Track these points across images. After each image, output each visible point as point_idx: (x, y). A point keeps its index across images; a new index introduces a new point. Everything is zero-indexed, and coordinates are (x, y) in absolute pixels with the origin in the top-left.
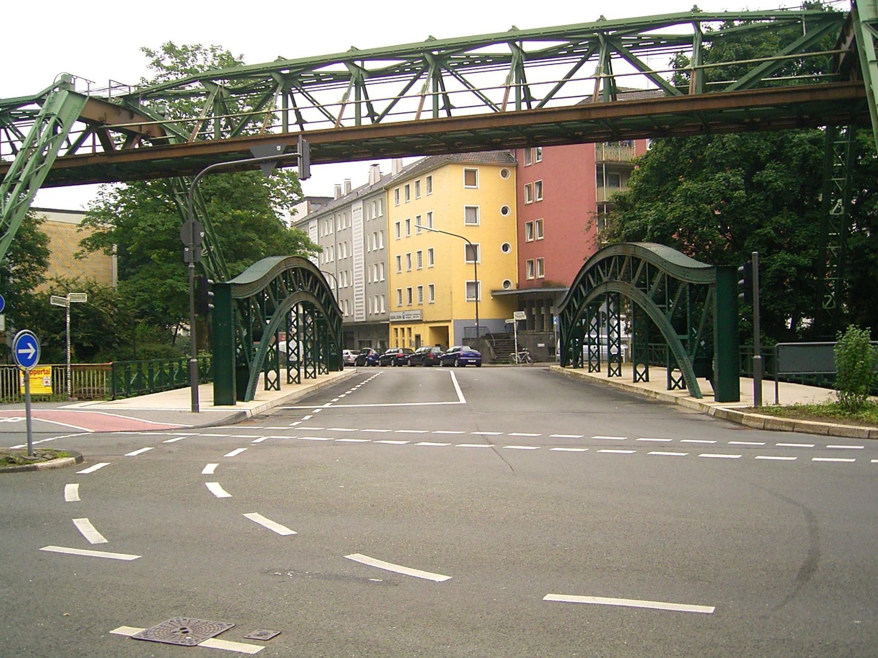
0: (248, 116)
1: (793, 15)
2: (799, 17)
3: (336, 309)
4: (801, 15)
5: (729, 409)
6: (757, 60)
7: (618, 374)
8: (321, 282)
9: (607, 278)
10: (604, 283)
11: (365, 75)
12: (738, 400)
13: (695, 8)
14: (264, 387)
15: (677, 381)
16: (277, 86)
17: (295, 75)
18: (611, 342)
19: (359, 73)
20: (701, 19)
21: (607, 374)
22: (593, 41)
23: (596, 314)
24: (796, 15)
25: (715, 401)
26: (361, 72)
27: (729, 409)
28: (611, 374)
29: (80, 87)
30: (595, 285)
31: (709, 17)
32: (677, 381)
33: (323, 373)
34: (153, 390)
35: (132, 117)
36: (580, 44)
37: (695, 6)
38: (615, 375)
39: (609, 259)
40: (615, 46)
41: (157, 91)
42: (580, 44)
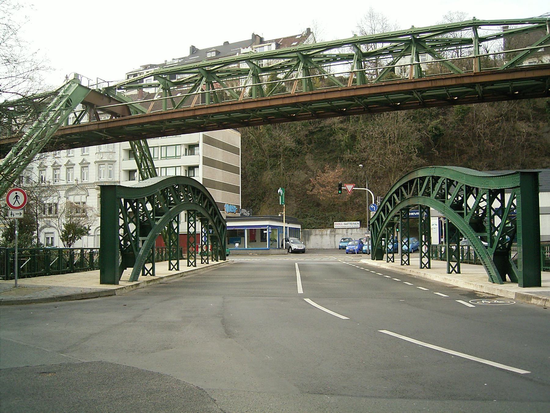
0: (185, 96)
1: (540, 21)
2: (544, 22)
3: (220, 217)
4: (545, 21)
5: (527, 292)
6: (100, 133)
7: (407, 264)
8: (208, 198)
9: (409, 195)
10: (407, 199)
11: (258, 70)
12: (539, 285)
13: (474, 19)
14: (168, 269)
15: (174, 265)
16: (203, 78)
17: (214, 71)
18: (176, 244)
19: (255, 68)
20: (479, 24)
21: (400, 263)
22: (407, 42)
23: (423, 221)
24: (543, 20)
25: (519, 286)
26: (256, 68)
27: (527, 292)
28: (403, 264)
29: (84, 83)
30: (400, 202)
31: (485, 23)
32: (174, 265)
33: (390, 261)
34: (73, 270)
35: (110, 102)
36: (337, 59)
37: (474, 18)
38: (405, 264)
39: (412, 182)
40: (422, 44)
41: (127, 84)
42: (337, 59)
